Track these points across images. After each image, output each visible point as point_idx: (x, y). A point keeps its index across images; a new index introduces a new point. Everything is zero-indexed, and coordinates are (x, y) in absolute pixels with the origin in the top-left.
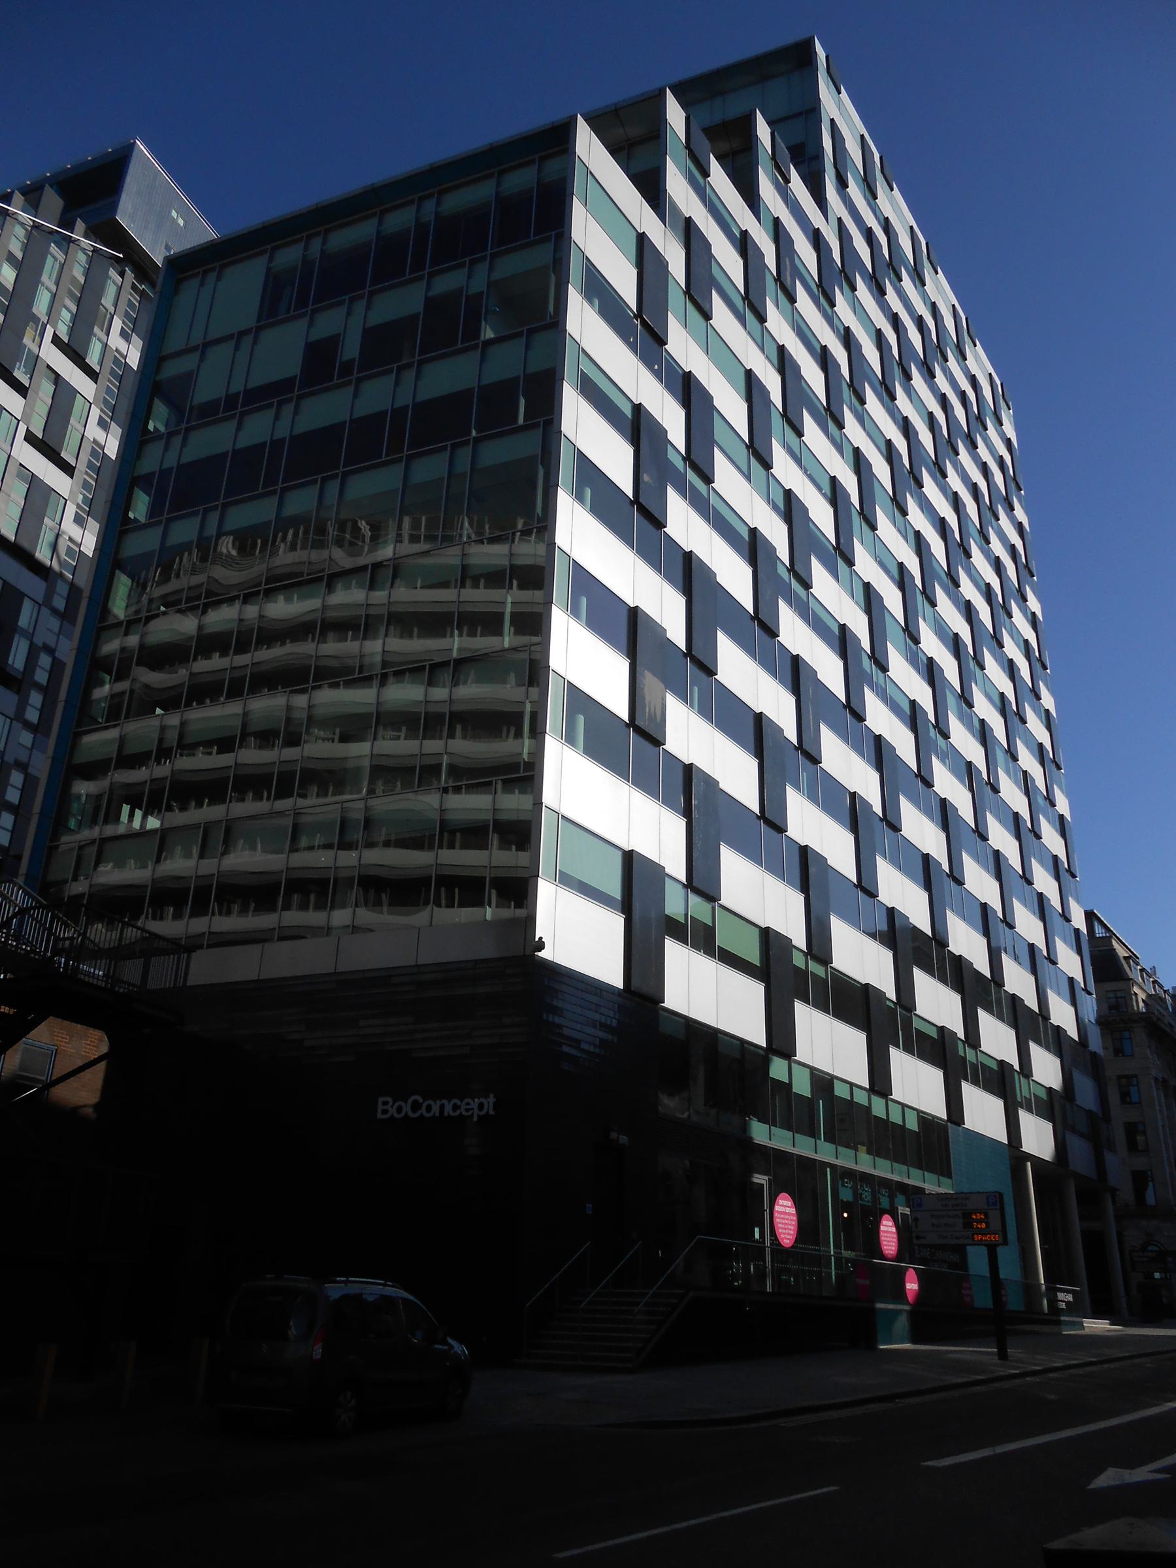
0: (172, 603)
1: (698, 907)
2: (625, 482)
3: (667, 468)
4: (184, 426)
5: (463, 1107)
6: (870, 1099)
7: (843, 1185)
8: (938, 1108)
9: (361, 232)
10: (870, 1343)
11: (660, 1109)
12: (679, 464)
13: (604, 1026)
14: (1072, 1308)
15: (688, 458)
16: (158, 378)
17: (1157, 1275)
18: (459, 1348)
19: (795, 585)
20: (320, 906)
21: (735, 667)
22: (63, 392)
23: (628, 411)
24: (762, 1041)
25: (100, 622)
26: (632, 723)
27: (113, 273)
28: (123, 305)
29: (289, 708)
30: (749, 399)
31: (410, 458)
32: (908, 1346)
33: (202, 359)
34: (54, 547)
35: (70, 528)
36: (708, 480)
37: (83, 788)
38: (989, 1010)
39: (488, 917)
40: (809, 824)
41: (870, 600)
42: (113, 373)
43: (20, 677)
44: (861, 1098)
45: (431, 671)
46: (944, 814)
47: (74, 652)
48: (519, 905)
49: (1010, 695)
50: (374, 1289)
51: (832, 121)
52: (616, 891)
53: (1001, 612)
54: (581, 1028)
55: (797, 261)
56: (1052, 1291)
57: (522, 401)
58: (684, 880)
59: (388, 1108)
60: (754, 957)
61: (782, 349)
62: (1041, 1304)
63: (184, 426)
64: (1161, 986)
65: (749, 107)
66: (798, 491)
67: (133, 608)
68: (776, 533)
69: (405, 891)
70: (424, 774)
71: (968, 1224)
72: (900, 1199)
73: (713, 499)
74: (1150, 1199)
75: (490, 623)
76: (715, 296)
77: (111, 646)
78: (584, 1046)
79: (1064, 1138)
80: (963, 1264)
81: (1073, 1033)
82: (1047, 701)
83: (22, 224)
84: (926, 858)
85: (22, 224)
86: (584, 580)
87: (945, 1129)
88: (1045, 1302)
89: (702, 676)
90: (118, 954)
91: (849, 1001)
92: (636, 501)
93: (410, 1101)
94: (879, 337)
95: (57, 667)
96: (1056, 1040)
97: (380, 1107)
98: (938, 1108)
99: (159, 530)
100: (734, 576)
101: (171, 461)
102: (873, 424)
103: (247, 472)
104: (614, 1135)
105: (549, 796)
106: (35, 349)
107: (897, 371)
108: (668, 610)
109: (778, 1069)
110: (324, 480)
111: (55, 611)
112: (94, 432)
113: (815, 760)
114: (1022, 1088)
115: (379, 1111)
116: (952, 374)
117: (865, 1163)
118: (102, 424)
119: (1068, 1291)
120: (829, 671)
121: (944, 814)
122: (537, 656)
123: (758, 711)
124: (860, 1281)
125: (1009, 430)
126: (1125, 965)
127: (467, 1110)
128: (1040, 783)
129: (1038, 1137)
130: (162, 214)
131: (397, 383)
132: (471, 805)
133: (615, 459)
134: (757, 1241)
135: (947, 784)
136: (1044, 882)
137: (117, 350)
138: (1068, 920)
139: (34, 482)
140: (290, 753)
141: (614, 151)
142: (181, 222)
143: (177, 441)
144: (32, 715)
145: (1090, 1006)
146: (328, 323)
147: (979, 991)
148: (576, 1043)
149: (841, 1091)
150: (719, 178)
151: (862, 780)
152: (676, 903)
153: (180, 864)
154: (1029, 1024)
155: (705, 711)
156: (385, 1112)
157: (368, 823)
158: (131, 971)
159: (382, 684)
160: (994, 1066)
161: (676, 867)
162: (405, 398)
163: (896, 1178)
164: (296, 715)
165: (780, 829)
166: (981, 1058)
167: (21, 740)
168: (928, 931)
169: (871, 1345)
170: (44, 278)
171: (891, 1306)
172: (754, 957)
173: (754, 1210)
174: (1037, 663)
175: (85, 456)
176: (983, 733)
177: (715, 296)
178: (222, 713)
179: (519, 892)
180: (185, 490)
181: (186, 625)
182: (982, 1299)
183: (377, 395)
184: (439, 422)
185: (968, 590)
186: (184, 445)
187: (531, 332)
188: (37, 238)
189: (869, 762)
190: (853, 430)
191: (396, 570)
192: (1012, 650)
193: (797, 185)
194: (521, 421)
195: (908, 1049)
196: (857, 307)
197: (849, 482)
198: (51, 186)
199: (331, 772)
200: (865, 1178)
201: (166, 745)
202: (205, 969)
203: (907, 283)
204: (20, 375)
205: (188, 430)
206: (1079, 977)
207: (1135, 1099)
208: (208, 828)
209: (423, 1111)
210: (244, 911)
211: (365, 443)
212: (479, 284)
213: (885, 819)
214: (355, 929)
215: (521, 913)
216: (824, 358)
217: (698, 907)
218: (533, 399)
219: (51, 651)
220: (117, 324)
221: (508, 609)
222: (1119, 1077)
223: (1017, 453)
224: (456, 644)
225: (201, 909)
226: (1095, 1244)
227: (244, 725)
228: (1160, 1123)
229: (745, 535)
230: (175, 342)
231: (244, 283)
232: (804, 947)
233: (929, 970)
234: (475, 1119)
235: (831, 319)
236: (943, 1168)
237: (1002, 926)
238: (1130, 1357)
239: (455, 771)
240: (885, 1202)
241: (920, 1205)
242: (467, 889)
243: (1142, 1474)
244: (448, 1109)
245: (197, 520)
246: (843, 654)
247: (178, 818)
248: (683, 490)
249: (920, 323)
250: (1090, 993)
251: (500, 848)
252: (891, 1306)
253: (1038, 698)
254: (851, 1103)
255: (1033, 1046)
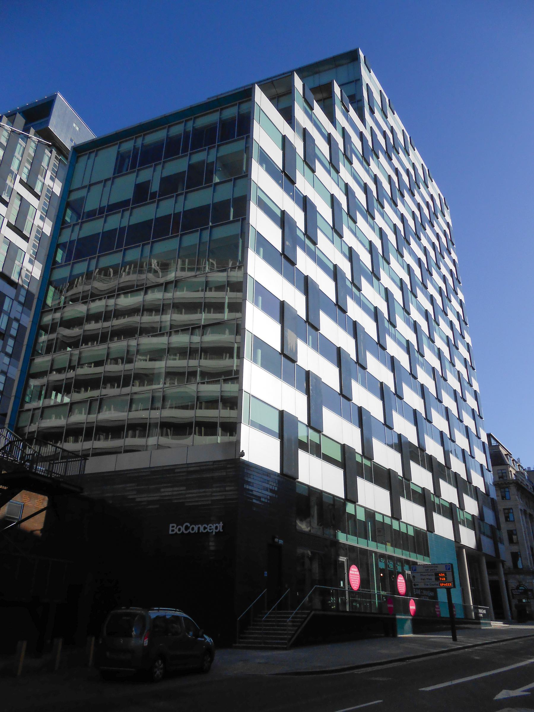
0: (75, 300)
1: (314, 436)
2: (278, 246)
3: (296, 238)
4: (80, 221)
5: (209, 528)
6: (392, 523)
7: (380, 561)
8: (422, 525)
9: (159, 135)
10: (394, 634)
11: (297, 527)
12: (302, 236)
13: (272, 491)
14: (486, 616)
15: (306, 234)
16: (69, 200)
17: (524, 601)
18: (208, 639)
19: (354, 290)
20: (141, 436)
21: (329, 327)
22: (24, 204)
23: (279, 213)
24: (342, 495)
25: (43, 309)
26: (282, 353)
27: (47, 152)
28: (51, 166)
29: (128, 346)
30: (333, 207)
31: (182, 235)
32: (411, 635)
33: (88, 192)
34: (20, 274)
35: (27, 265)
36: (315, 243)
37: (33, 383)
38: (445, 480)
39: (219, 442)
40: (363, 397)
41: (388, 295)
42: (46, 195)
43: (4, 332)
44: (388, 521)
45: (192, 328)
46: (423, 391)
47: (31, 323)
48: (231, 435)
49: (451, 337)
50: (170, 613)
51: (367, 84)
52: (276, 429)
53: (446, 299)
54: (259, 490)
55: (353, 146)
56: (476, 609)
57: (232, 210)
58: (306, 423)
59: (174, 529)
60: (339, 458)
61: (346, 185)
62: (472, 615)
63: (80, 221)
64: (522, 467)
65: (331, 78)
66: (355, 248)
67: (57, 302)
68: (345, 266)
69: (180, 429)
70: (190, 375)
71: (437, 579)
72: (406, 567)
73: (318, 252)
74: (520, 566)
75: (218, 307)
76: (317, 162)
77: (47, 319)
78: (263, 500)
79: (480, 538)
80: (435, 597)
81: (483, 489)
82: (468, 339)
83: (7, 130)
84: (415, 411)
85: (7, 130)
86: (260, 289)
87: (426, 534)
88: (473, 613)
89: (313, 331)
90: (52, 459)
91: (382, 477)
92: (283, 254)
93: (184, 526)
94: (390, 178)
95: (21, 329)
96: (475, 493)
97: (171, 529)
98: (422, 525)
99: (69, 267)
100: (327, 286)
101: (75, 237)
102: (388, 218)
103: (109, 241)
104: (276, 540)
105: (246, 387)
106: (12, 186)
107: (398, 193)
108: (297, 302)
109: (350, 508)
110: (143, 245)
111: (20, 303)
112: (38, 222)
113: (364, 368)
114: (460, 515)
115: (170, 531)
116: (422, 194)
117: (389, 550)
118: (42, 218)
119: (484, 609)
120: (370, 327)
121: (423, 391)
122: (239, 322)
123: (338, 346)
124: (389, 606)
125: (448, 219)
126: (506, 458)
127: (210, 529)
128: (465, 376)
129: (468, 538)
130: (70, 127)
131: (176, 202)
132: (211, 389)
133: (273, 235)
134: (342, 588)
135: (424, 378)
136: (468, 421)
137: (48, 186)
138: (479, 438)
139: (11, 245)
140: (128, 366)
141: (271, 99)
142: (77, 129)
143: (77, 228)
144: (9, 350)
145: (490, 477)
146: (145, 175)
147: (439, 471)
148: (258, 498)
149: (378, 518)
150: (318, 110)
151: (386, 377)
152: (303, 433)
153: (79, 417)
154: (463, 486)
155: (315, 347)
156: (173, 531)
157: (164, 398)
158: (59, 469)
159: (170, 335)
160: (447, 505)
161: (303, 417)
162: (179, 209)
163: (404, 557)
164: (131, 349)
165: (349, 399)
166: (442, 502)
167: (4, 361)
168: (417, 445)
169: (394, 635)
170: (16, 154)
171: (403, 617)
172: (339, 458)
173: (339, 573)
174: (463, 322)
175: (34, 233)
176: (439, 354)
177: (317, 162)
178: (97, 350)
179: (232, 428)
180: (82, 250)
181: (81, 309)
182: (445, 613)
183: (167, 207)
184: (195, 220)
185: (431, 290)
186: (80, 229)
187: (235, 179)
188: (13, 136)
189: (388, 368)
190: (379, 220)
191: (176, 283)
192: (452, 317)
193: (352, 113)
194: (231, 219)
195: (409, 498)
196: (379, 165)
197: (378, 243)
198: (19, 113)
199: (146, 375)
200: (390, 557)
201: (72, 364)
202: (93, 466)
203: (401, 155)
204: (5, 197)
205: (82, 223)
206: (485, 464)
207: (512, 519)
208: (92, 401)
209: (190, 530)
210: (106, 438)
211: (161, 228)
212: (212, 158)
213: (396, 394)
214: (159, 447)
215: (233, 439)
216: (365, 189)
217: (314, 436)
218: (237, 208)
219: (17, 320)
220: (49, 174)
221: (227, 301)
222: (504, 509)
223: (452, 229)
224: (203, 317)
225: (88, 437)
226: (495, 587)
227: (108, 354)
228: (523, 530)
229: (332, 267)
230: (76, 184)
231: (108, 158)
232: (361, 453)
233: (417, 462)
234: (214, 533)
235: (368, 171)
236: (426, 553)
237: (449, 441)
238: (512, 639)
239: (204, 374)
240: (399, 569)
241: (415, 570)
242: (208, 428)
243: (518, 692)
244: (202, 529)
245: (86, 263)
246: (376, 320)
247: (77, 397)
248: (304, 248)
249: (408, 172)
250: (490, 471)
251: (223, 409)
252: (403, 617)
253: (464, 338)
254: (383, 523)
255: (465, 496)
